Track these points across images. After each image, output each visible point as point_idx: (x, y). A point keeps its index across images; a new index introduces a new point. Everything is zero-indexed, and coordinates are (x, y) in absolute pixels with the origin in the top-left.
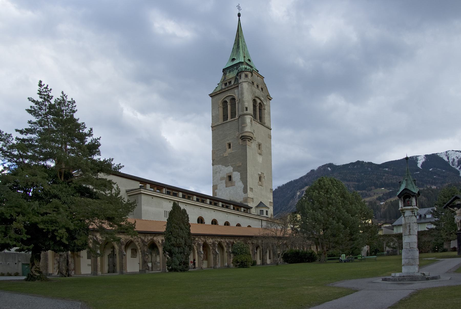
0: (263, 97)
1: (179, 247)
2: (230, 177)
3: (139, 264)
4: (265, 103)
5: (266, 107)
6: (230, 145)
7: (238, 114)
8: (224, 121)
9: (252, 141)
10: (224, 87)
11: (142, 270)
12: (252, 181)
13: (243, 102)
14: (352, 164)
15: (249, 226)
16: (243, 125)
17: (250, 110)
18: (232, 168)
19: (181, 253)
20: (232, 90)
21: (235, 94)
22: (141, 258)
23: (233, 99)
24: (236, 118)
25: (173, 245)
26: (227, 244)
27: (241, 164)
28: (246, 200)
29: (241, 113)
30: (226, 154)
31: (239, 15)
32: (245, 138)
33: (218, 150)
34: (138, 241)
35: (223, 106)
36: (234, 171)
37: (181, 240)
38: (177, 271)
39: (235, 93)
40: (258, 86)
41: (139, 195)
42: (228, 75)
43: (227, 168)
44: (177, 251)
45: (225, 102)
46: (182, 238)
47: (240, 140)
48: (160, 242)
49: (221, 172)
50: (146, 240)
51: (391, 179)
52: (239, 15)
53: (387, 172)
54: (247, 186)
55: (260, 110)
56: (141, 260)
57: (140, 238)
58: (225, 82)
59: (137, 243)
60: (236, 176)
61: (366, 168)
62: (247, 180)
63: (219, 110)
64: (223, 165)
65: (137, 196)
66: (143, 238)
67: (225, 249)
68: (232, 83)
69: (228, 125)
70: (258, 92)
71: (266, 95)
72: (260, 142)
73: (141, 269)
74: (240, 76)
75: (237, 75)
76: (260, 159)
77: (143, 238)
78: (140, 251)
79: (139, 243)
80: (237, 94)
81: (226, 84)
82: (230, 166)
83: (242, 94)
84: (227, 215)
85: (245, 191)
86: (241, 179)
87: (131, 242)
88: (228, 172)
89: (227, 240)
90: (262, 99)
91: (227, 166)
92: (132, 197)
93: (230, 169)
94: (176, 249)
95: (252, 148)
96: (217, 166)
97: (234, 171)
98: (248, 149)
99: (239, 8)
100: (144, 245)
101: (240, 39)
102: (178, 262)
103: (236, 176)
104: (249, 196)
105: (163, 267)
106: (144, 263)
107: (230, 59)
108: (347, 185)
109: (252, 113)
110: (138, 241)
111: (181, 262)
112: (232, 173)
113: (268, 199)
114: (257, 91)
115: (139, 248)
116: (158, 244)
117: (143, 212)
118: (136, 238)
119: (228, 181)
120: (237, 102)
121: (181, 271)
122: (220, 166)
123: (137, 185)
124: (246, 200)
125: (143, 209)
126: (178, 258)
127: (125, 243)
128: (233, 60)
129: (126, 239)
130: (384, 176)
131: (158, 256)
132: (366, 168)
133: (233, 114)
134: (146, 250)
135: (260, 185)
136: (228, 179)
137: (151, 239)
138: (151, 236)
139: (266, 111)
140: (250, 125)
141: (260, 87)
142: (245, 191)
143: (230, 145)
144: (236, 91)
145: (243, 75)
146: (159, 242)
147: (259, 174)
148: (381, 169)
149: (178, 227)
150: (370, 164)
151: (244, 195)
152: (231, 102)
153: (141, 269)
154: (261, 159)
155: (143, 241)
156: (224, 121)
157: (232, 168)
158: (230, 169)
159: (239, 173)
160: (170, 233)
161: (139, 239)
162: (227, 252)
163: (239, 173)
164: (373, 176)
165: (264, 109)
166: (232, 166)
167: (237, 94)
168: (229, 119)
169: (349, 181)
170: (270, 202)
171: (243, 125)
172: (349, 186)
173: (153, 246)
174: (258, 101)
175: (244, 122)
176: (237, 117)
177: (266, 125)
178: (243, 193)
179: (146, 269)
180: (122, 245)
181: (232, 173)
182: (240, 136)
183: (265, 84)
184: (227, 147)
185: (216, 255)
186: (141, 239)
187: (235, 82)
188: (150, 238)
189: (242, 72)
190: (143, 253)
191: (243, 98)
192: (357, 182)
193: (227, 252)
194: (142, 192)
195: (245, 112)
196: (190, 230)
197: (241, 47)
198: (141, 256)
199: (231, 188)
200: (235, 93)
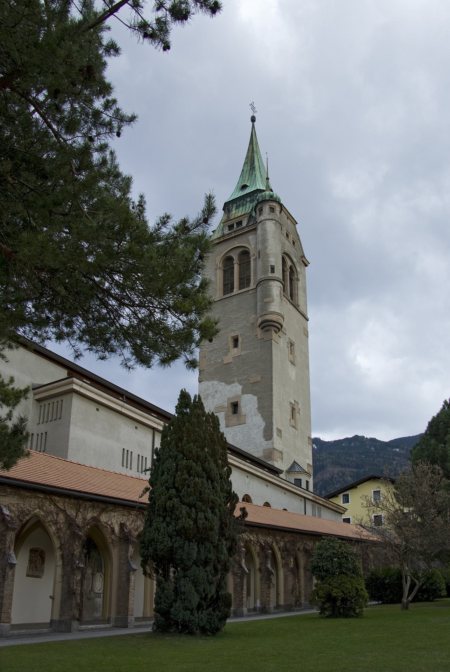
0: (295, 257)
1: (201, 541)
2: (235, 406)
3: (52, 598)
4: (298, 269)
5: (300, 277)
6: (236, 341)
7: (255, 280)
8: (224, 294)
9: (280, 333)
10: (227, 231)
11: (60, 622)
12: (280, 416)
13: (267, 255)
14: (347, 439)
15: (285, 509)
16: (266, 300)
17: (278, 274)
18: (240, 387)
19: (206, 563)
20: (244, 238)
21: (250, 244)
22: (59, 579)
23: (245, 253)
24: (250, 288)
25: (182, 533)
26: (262, 548)
27: (259, 379)
28: (270, 453)
29: (260, 276)
30: (228, 359)
31: (253, 119)
32: (270, 326)
33: (211, 351)
34: (56, 523)
35: (225, 266)
36: (244, 392)
37: (210, 515)
38: (191, 633)
39: (250, 242)
40: (287, 235)
41: (65, 398)
42: (234, 212)
43: (229, 387)
44: (195, 556)
45: (228, 260)
46: (212, 509)
47: (259, 331)
48: (117, 529)
49: (217, 396)
50: (79, 521)
51: (405, 466)
52: (253, 119)
53: (398, 455)
54: (272, 424)
55: (291, 280)
56: (59, 586)
57: (64, 511)
58: (230, 223)
59: (53, 529)
60: (249, 403)
61: (368, 447)
62: (272, 411)
63: (216, 275)
64: (220, 380)
65: (59, 399)
66: (72, 513)
67: (257, 561)
68: (244, 224)
69: (235, 301)
70: (289, 249)
71: (300, 256)
72: (293, 339)
73: (56, 617)
74: (261, 210)
75: (255, 209)
76: (292, 372)
77: (72, 513)
78: (58, 553)
79: (58, 530)
80: (252, 243)
81: (231, 227)
82: (237, 384)
83: (264, 241)
84: (247, 480)
85: (268, 434)
86: (259, 409)
87: (38, 524)
88: (231, 396)
89: (262, 539)
90: (295, 260)
91: (229, 383)
92: (46, 403)
93: (237, 388)
94: (193, 550)
95: (279, 346)
96: (209, 383)
97: (244, 392)
98: (274, 348)
99: (253, 108)
100: (74, 535)
101: (256, 156)
102: (196, 599)
103: (249, 403)
104: (275, 446)
105: (118, 613)
106: (68, 593)
107: (237, 187)
108: (342, 472)
109: (281, 277)
110: (56, 523)
111: (205, 599)
112: (239, 397)
113: (306, 460)
114: (287, 243)
115: (57, 544)
116: (109, 538)
117: (71, 444)
118: (51, 512)
119: (230, 413)
120: (252, 259)
121: (204, 631)
122: (215, 382)
123: (63, 373)
124: (270, 453)
125: (71, 435)
126: (195, 584)
127: (17, 525)
128: (244, 187)
129: (22, 512)
130: (395, 460)
131: (98, 575)
132: (368, 447)
133: (245, 281)
134: (77, 552)
135: (293, 427)
136: (231, 410)
137: (93, 518)
138: (93, 507)
139: (300, 284)
140: (278, 305)
141: (291, 236)
142: (268, 434)
143: (236, 341)
144: (251, 237)
145: (266, 209)
146: (113, 530)
147: (291, 403)
148: (389, 449)
149: (200, 469)
150: (373, 440)
151: (265, 444)
152: (240, 259)
153: (56, 617)
154: (294, 373)
155: (70, 523)
156: (224, 294)
157: (240, 387)
158: (237, 388)
159: (255, 398)
160: (173, 491)
161: (61, 516)
162: (260, 570)
163: (255, 398)
164: (379, 459)
165: (298, 280)
166: (240, 382)
167: (252, 243)
168: (236, 291)
169: (344, 466)
170: (308, 465)
171: (266, 300)
172: (344, 474)
173: (93, 545)
174: (289, 263)
175: (267, 294)
176: (252, 286)
177: (301, 308)
178: (263, 440)
179: (74, 618)
180: (8, 529)
181: (239, 397)
182: (260, 321)
183: (298, 236)
184: (231, 344)
185: (242, 578)
186: (67, 516)
187: (248, 223)
188: (89, 516)
189: (264, 201)
190: (68, 562)
191: (266, 248)
192: (356, 468)
193: (260, 570)
194: (75, 387)
195: (270, 275)
196: (230, 484)
197: (257, 167)
198: (59, 571)
199: (237, 428)
200: (250, 242)
